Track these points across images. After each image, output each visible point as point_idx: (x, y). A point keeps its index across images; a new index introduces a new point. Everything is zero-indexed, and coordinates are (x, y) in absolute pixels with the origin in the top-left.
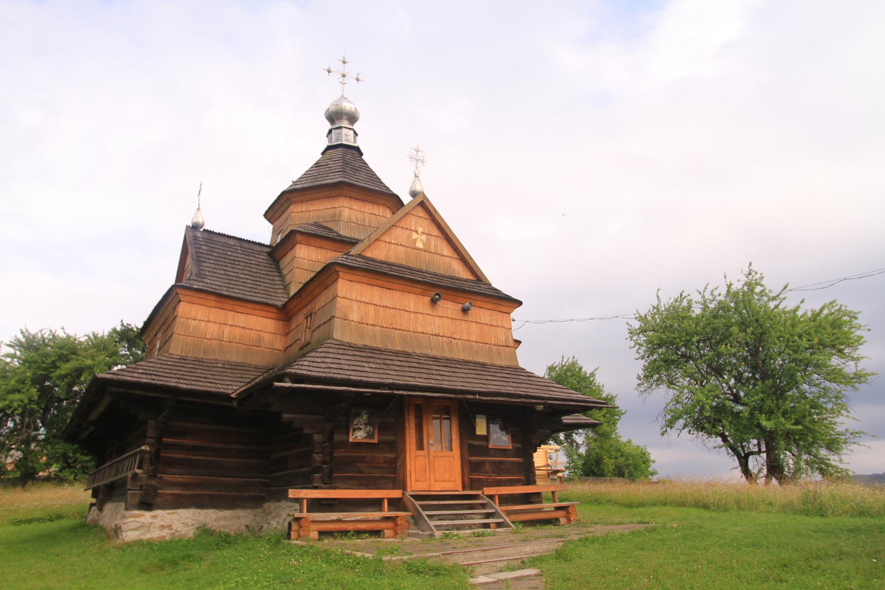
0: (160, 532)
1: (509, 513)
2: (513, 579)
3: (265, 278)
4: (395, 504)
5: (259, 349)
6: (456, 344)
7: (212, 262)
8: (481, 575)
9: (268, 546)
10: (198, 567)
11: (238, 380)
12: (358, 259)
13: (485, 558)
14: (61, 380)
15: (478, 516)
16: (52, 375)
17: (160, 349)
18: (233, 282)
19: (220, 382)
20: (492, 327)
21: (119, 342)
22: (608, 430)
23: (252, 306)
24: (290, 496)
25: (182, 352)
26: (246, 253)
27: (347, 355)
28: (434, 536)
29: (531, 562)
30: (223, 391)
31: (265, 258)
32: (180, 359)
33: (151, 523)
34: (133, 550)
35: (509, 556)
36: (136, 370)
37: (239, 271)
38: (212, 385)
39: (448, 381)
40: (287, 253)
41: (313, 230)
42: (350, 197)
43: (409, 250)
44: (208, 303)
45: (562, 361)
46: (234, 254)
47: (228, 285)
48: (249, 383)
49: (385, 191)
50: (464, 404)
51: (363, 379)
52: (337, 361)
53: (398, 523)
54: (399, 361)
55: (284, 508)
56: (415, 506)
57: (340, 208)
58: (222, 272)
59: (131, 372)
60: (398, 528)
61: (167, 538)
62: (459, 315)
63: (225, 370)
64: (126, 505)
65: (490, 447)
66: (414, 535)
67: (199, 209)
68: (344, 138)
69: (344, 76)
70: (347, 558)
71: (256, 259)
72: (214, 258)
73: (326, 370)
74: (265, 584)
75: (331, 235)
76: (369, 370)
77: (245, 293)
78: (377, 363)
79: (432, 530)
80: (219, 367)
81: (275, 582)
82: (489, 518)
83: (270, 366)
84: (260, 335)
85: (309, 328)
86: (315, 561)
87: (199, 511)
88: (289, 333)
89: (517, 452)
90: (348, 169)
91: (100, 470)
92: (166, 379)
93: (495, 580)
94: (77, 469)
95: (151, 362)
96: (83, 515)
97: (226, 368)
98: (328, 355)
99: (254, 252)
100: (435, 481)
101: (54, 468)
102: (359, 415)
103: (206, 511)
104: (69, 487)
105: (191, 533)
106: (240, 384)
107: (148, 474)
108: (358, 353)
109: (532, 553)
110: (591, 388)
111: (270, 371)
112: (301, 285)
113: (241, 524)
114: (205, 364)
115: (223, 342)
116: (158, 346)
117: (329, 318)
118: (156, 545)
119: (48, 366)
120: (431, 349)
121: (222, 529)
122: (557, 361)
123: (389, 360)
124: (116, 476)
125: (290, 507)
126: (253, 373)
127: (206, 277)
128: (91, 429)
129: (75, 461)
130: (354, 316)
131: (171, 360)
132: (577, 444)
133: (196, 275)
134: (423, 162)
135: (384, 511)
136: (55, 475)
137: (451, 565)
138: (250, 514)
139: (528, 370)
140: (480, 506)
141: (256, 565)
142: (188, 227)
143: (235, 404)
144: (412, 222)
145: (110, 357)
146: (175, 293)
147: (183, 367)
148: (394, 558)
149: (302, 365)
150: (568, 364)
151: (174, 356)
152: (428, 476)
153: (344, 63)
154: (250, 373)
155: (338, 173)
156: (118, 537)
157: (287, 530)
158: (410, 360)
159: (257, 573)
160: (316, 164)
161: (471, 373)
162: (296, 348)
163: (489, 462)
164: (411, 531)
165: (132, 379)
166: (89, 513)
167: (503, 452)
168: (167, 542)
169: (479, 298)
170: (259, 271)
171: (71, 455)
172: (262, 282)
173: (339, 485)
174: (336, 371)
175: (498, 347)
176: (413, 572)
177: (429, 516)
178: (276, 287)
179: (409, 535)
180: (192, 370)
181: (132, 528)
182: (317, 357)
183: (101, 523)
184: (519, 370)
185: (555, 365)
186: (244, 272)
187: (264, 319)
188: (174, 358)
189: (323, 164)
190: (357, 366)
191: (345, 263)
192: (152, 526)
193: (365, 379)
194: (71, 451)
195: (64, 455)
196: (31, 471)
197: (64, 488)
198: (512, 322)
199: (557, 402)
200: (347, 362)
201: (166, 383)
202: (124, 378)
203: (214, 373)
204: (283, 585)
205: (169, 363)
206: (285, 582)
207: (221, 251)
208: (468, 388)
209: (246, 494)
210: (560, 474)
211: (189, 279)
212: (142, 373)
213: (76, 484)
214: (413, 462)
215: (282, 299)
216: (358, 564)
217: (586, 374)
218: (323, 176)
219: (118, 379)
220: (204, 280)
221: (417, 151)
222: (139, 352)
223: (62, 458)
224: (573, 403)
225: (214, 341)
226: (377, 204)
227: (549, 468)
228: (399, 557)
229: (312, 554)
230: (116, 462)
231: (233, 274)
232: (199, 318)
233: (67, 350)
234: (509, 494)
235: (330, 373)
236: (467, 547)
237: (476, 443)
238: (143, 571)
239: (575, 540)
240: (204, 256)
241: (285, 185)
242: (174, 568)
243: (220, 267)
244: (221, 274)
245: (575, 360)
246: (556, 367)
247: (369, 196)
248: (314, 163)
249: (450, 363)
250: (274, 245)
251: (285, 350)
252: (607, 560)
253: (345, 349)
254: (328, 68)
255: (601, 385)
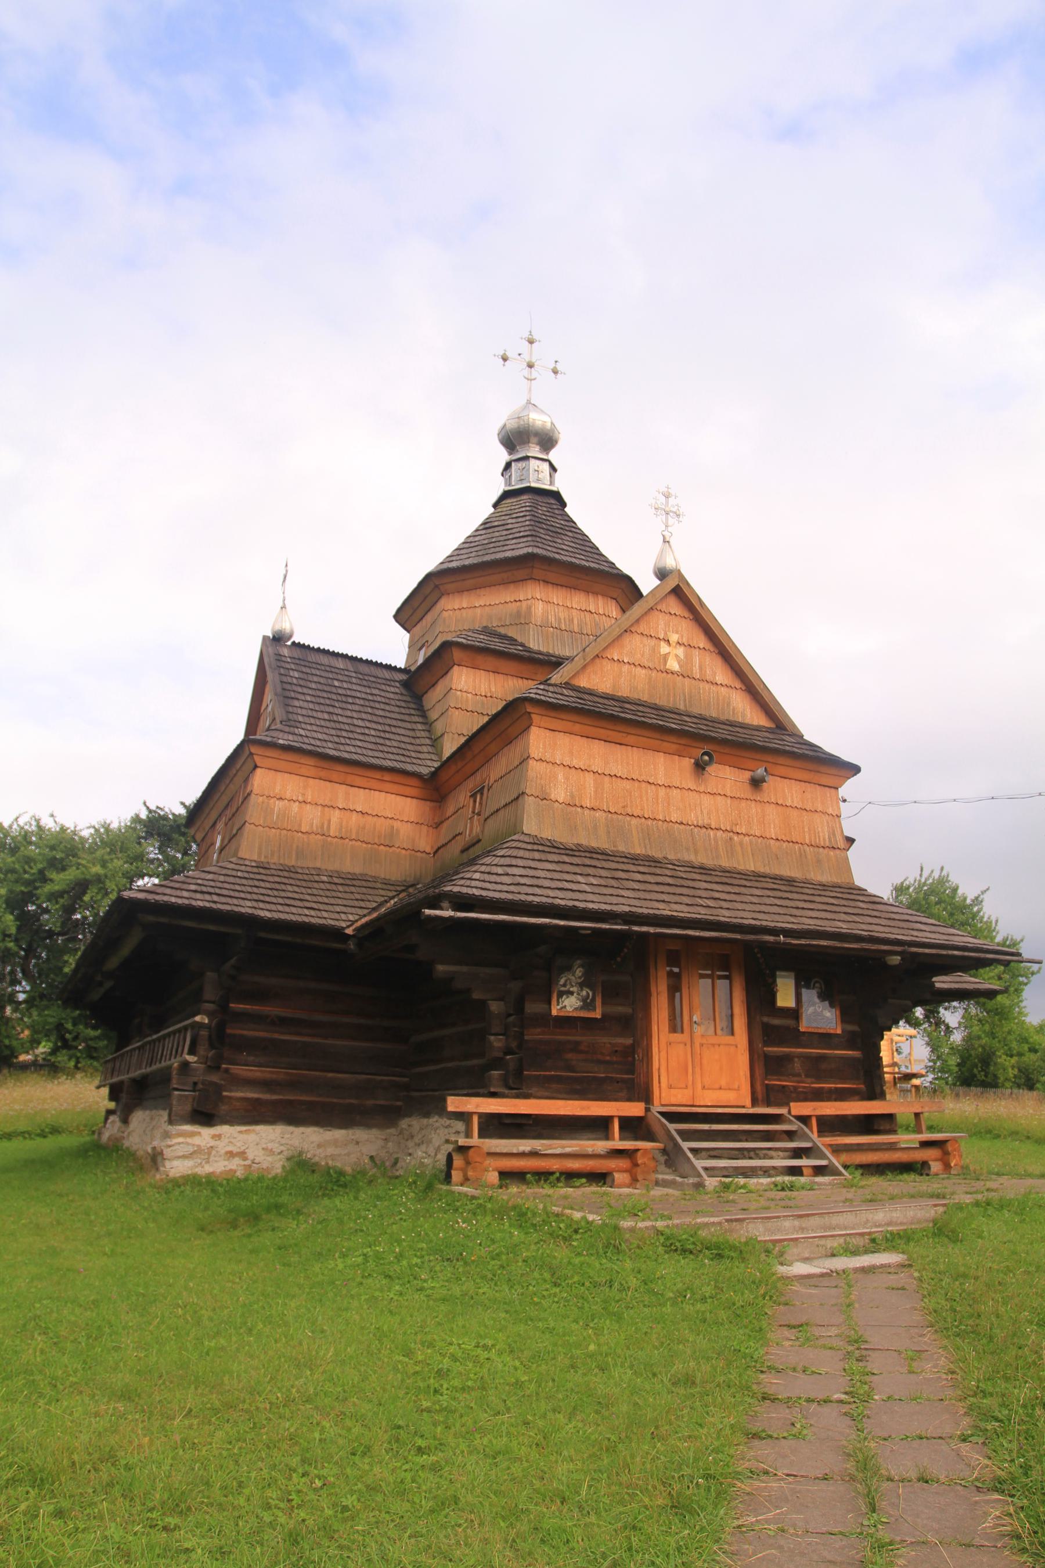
0: (226, 1163)
1: (837, 1150)
2: (856, 1270)
3: (399, 727)
4: (633, 1127)
5: (391, 850)
6: (741, 843)
7: (309, 698)
8: (797, 1261)
9: (412, 1195)
10: (295, 1226)
11: (356, 903)
12: (565, 692)
13: (802, 1229)
14: (54, 901)
15: (781, 1154)
16: (39, 892)
17: (222, 849)
18: (344, 734)
19: (326, 907)
20: (805, 813)
21: (145, 838)
22: (1007, 1002)
23: (378, 775)
24: (451, 1108)
25: (260, 854)
26: (365, 683)
27: (547, 861)
28: (704, 1186)
29: (887, 1240)
30: (332, 923)
31: (397, 690)
32: (632, 859)
33: (212, 1147)
34: (182, 1192)
35: (846, 1228)
36: (185, 886)
37: (355, 715)
38: (313, 913)
39: (728, 909)
40: (437, 682)
41: (482, 640)
42: (546, 582)
43: (654, 674)
44: (304, 770)
45: (921, 875)
46: (345, 685)
47: (336, 739)
48: (374, 909)
49: (607, 569)
50: (756, 950)
51: (577, 904)
52: (531, 873)
53: (640, 1162)
54: (639, 872)
55: (436, 1129)
56: (668, 1131)
57: (529, 602)
58: (326, 716)
59: (177, 889)
60: (639, 1170)
61: (239, 1174)
62: (746, 791)
63: (334, 887)
64: (170, 1115)
65: (802, 1029)
66: (666, 1184)
67: (283, 607)
68: (532, 476)
69: (531, 366)
70: (555, 1221)
71: (383, 694)
72: (310, 692)
73: (512, 888)
74: (415, 1260)
75: (512, 649)
76: (588, 888)
77: (365, 752)
78: (600, 877)
79: (700, 1176)
80: (323, 882)
81: (432, 1258)
82: (801, 1158)
83: (410, 880)
84: (393, 827)
85: (479, 814)
86: (498, 1224)
87: (291, 1128)
88: (442, 822)
89: (850, 1040)
90: (542, 531)
91: (122, 1055)
92: (235, 901)
93: (825, 1271)
94: (80, 1051)
95: (209, 872)
96: (94, 1129)
97: (336, 884)
98: (514, 862)
99: (379, 681)
100: (704, 1088)
101: (43, 1048)
102: (569, 968)
103: (302, 1129)
104: (68, 1081)
105: (276, 1165)
106: (361, 912)
107: (206, 1063)
108: (566, 859)
109: (889, 1224)
110: (975, 926)
111: (411, 890)
112: (463, 740)
113: (363, 1154)
114: (300, 877)
115: (329, 839)
116: (218, 844)
117: (515, 796)
118: (221, 1185)
119: (32, 878)
120: (696, 852)
121: (330, 1163)
122: (910, 875)
123: (622, 871)
124: (151, 1066)
125: (446, 1127)
126: (382, 892)
127: (298, 725)
128: (109, 984)
129: (76, 1038)
130: (559, 793)
131: (243, 868)
132: (947, 1027)
133: (281, 722)
134: (678, 516)
135: (614, 1139)
136: (44, 1059)
137: (743, 1240)
138: (377, 1138)
139: (871, 890)
140: (785, 1136)
141: (394, 1226)
142: (265, 638)
143: (352, 947)
144: (659, 623)
145: (131, 864)
146: (247, 753)
147: (263, 880)
148: (640, 1225)
149: (470, 879)
150: (931, 881)
151: (247, 863)
152: (690, 1077)
153: (531, 342)
154: (376, 892)
155: (525, 539)
156: (157, 1169)
157: (444, 1168)
158: (658, 871)
159: (399, 1241)
160: (484, 523)
161: (769, 896)
162: (456, 848)
163: (801, 1056)
164: (660, 1177)
165: (180, 901)
166: (105, 1126)
167: (825, 1039)
168: (239, 1181)
169: (781, 760)
170: (388, 714)
171: (69, 1026)
172: (394, 733)
173: (533, 1091)
174: (530, 890)
175: (816, 849)
176: (676, 1250)
177: (694, 1150)
178: (418, 741)
179: (657, 1183)
180: (277, 886)
181: (181, 1154)
182: (496, 865)
183: (126, 1143)
184: (855, 892)
185: (907, 882)
186: (364, 716)
187: (399, 798)
188: (246, 865)
189: (496, 524)
190: (566, 881)
191: (543, 698)
192: (214, 1152)
193: (581, 905)
194: (70, 1021)
195: (59, 1027)
196: (7, 1052)
197: (59, 1083)
198: (841, 804)
199: (927, 951)
200: (549, 875)
201: (236, 909)
202: (166, 898)
203: (315, 892)
204: (445, 1264)
205: (239, 874)
206: (448, 1260)
207: (322, 680)
208: (764, 923)
209: (370, 1102)
210: (916, 1082)
211: (268, 730)
212: (195, 891)
213: (79, 1076)
214: (663, 1054)
215: (429, 763)
216: (576, 1231)
217: (965, 899)
218: (498, 544)
219: (157, 901)
220: (296, 731)
221: (667, 496)
222: (179, 856)
223: (55, 1032)
224: (956, 953)
225: (313, 836)
226: (593, 593)
227: (897, 1070)
228: (648, 1224)
229: (493, 1212)
230: (149, 1042)
231: (344, 720)
232: (288, 796)
233: (62, 852)
234: (837, 1116)
235: (519, 893)
236: (767, 1208)
237: (776, 1022)
238: (203, 1229)
239: (967, 1205)
240: (295, 688)
241: (430, 564)
242: (254, 1226)
243: (322, 708)
244: (324, 720)
245: (944, 873)
246: (908, 888)
247: (579, 578)
248: (480, 522)
249: (730, 877)
250: (413, 669)
251: (435, 853)
252: (1032, 1244)
253: (544, 851)
254: (501, 353)
255: (993, 918)
